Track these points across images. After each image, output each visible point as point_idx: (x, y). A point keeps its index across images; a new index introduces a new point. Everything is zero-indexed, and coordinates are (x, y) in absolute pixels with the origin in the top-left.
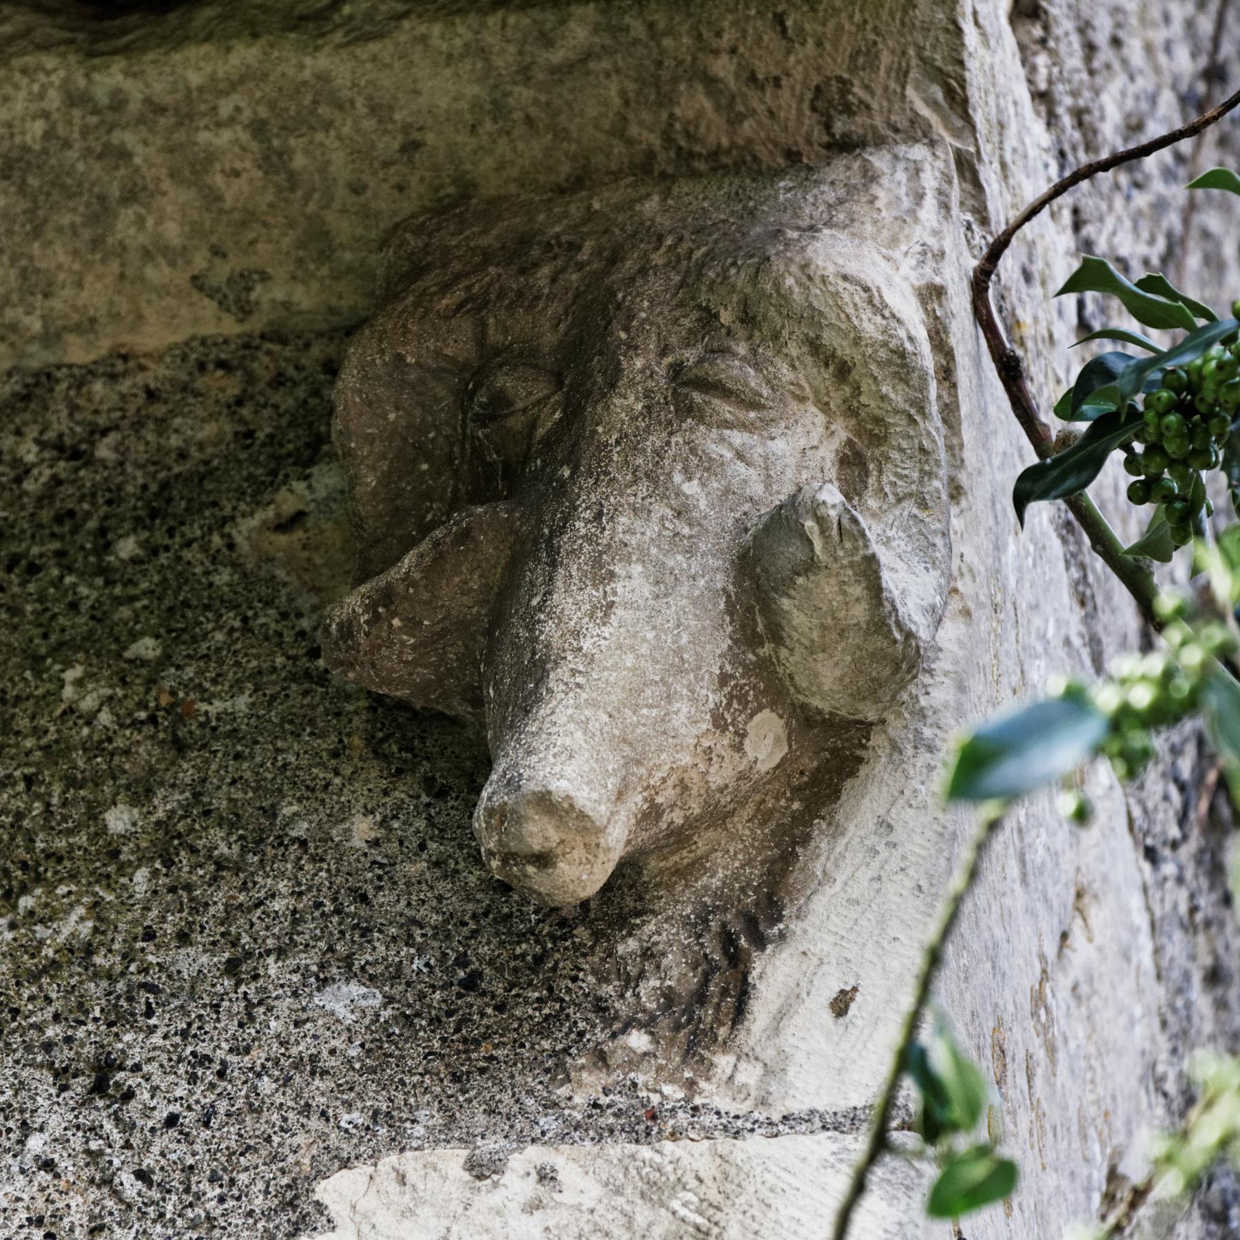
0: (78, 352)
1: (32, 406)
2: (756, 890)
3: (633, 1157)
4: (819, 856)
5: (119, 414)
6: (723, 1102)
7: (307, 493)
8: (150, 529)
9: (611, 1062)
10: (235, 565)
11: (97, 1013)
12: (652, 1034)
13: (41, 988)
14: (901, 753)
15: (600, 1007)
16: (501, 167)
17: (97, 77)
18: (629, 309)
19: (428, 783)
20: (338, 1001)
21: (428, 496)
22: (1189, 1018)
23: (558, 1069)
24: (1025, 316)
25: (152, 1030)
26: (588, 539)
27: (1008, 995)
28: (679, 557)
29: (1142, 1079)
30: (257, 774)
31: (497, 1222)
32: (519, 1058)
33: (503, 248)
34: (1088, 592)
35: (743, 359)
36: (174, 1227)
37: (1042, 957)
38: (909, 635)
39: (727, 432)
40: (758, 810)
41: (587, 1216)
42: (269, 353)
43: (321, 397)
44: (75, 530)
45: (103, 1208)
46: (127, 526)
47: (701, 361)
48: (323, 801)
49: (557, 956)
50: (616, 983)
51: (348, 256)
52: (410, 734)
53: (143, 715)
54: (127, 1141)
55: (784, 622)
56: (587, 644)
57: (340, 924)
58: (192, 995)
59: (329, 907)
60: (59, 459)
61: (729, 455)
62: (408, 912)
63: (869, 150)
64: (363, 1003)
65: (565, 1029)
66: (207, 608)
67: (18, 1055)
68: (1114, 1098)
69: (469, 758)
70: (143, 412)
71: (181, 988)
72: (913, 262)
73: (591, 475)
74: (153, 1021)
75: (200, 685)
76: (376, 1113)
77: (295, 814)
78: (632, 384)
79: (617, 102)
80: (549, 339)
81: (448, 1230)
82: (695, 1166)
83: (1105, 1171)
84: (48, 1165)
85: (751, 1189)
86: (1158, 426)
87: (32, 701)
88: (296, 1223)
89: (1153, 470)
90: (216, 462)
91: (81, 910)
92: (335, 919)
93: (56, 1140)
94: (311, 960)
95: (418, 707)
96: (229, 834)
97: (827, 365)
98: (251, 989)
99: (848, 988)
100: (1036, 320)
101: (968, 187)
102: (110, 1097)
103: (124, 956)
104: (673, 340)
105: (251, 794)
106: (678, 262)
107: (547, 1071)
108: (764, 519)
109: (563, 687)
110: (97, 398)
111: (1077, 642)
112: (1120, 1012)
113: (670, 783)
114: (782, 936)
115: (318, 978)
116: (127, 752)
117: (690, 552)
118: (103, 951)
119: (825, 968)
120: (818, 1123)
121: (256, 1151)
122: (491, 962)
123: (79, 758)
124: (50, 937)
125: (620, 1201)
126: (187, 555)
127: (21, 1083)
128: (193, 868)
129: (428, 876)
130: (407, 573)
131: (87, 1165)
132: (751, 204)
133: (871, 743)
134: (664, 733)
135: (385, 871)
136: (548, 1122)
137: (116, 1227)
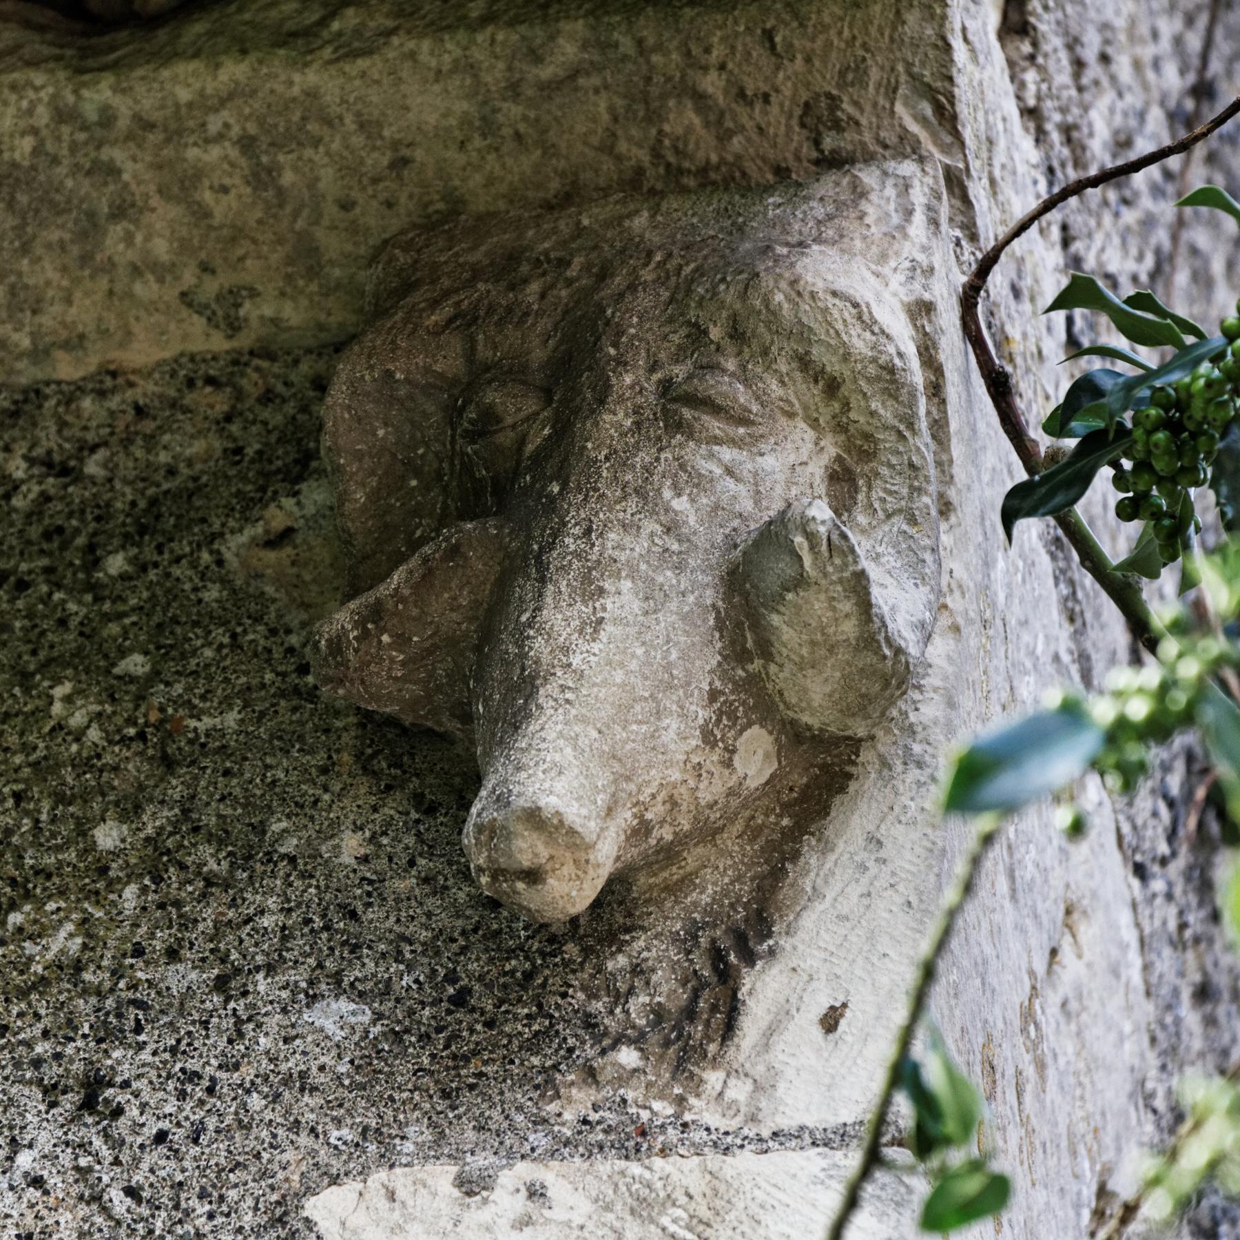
0: (67, 369)
1: (21, 422)
2: (746, 906)
3: (622, 1173)
5: (108, 430)
6: (713, 1119)
7: (295, 509)
8: (139, 545)
10: (225, 582)
11: (86, 1030)
12: (641, 1050)
13: (30, 1005)
15: (590, 1023)
16: (490, 181)
17: (86, 93)
19: (418, 799)
20: (327, 1018)
21: (416, 512)
22: (1178, 1034)
23: (547, 1085)
24: (1014, 332)
25: (141, 1046)
26: (577, 555)
27: (997, 1011)
28: (669, 573)
30: (247, 790)
32: (508, 1074)
33: (492, 264)
34: (1077, 609)
35: (733, 375)
37: (1032, 973)
38: (899, 651)
39: (716, 448)
40: (747, 826)
43: (310, 414)
44: (64, 547)
46: (116, 542)
47: (690, 377)
48: (312, 818)
49: (547, 972)
50: (606, 999)
51: (337, 272)
53: (132, 731)
54: (116, 1158)
55: (773, 638)
56: (576, 661)
57: (329, 940)
58: (182, 1011)
59: (318, 923)
60: (48, 475)
61: (718, 471)
63: (858, 166)
64: (353, 1020)
65: (555, 1046)
66: (196, 624)
67: (7, 1071)
68: (1103, 1114)
69: (457, 775)
71: (170, 1005)
72: (903, 278)
74: (142, 1038)
75: (189, 701)
76: (366, 1129)
77: (284, 831)
78: (621, 400)
79: (606, 117)
80: (538, 355)
82: (684, 1182)
84: (37, 1182)
85: (741, 1205)
86: (1147, 443)
87: (21, 718)
89: (1141, 487)
90: (204, 479)
91: (70, 927)
92: (325, 935)
93: (45, 1157)
94: (299, 977)
96: (218, 851)
97: (816, 381)
98: (240, 1005)
99: (838, 1004)
100: (1025, 335)
101: (958, 203)
102: (99, 1113)
103: (114, 973)
105: (240, 811)
106: (668, 278)
108: (753, 536)
109: (551, 703)
110: (86, 415)
111: (1066, 658)
112: (1109, 1029)
114: (772, 952)
115: (307, 995)
116: (115, 769)
117: (679, 568)
118: (92, 967)
119: (815, 984)
120: (808, 1140)
121: (246, 1167)
122: (481, 979)
123: (68, 775)
124: (40, 953)
125: (610, 1217)
126: (176, 571)
128: (182, 884)
129: (417, 891)
130: (396, 590)
131: (76, 1181)
132: (741, 220)
133: (861, 759)
134: (654, 749)
136: (538, 1139)
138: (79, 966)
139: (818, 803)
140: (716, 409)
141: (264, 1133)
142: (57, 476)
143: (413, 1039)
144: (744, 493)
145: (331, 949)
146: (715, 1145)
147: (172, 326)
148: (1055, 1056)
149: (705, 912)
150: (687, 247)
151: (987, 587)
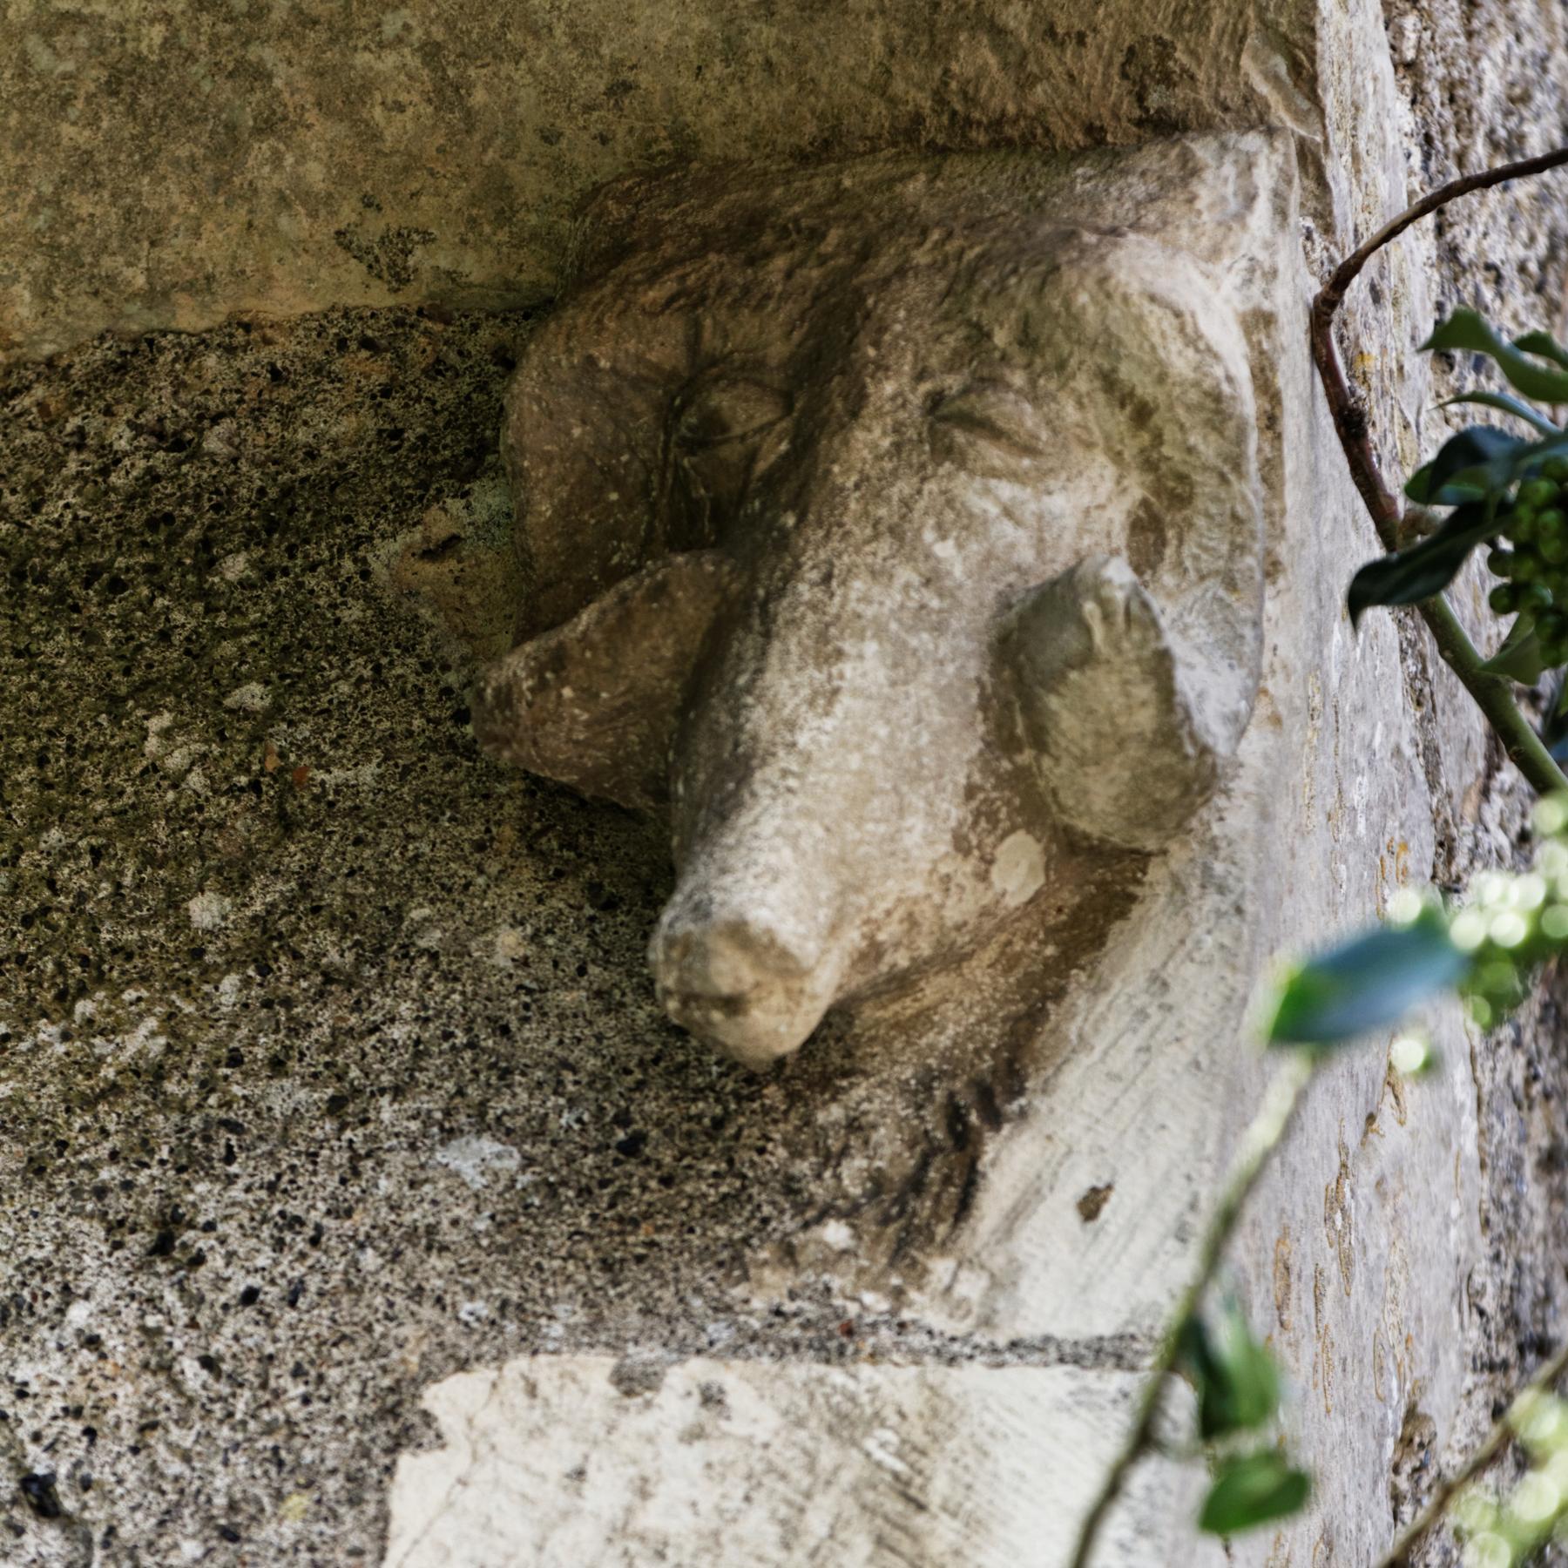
0: (189, 317)
2: (994, 1054)
3: (821, 1381)
4: (1074, 1016)
5: (236, 396)
6: (936, 1318)
7: (464, 513)
9: (801, 1259)
10: (369, 598)
11: (164, 1153)
12: (853, 1226)
13: (96, 1118)
14: (1184, 892)
15: (790, 1186)
16: (731, 120)
18: (881, 319)
19: (594, 889)
20: (465, 1159)
21: (614, 533)
22: (1517, 1216)
23: (735, 1263)
24: (1371, 346)
25: (231, 1180)
26: (814, 607)
27: (1297, 1196)
28: (925, 636)
29: (1456, 1293)
30: (382, 865)
31: (647, 1453)
32: (686, 1246)
33: (727, 229)
34: (1427, 690)
35: (1018, 392)
36: (245, 1430)
37: (1342, 1148)
38: (1204, 750)
39: (993, 482)
40: (1002, 953)
41: (759, 1452)
42: (426, 332)
43: (489, 394)
44: (171, 540)
45: (158, 1401)
46: (237, 539)
47: (966, 391)
48: (461, 905)
49: (742, 1120)
50: (813, 1159)
51: (533, 219)
52: (574, 828)
54: (193, 1319)
55: (1049, 725)
56: (803, 739)
57: (474, 1061)
58: (285, 1141)
59: (461, 1038)
60: (159, 448)
61: (994, 510)
62: (558, 1051)
63: (1190, 134)
64: (497, 1164)
65: (746, 1214)
66: (331, 650)
67: (63, 1201)
68: (1419, 1319)
69: (646, 863)
70: (266, 396)
71: (271, 1129)
72: (1238, 281)
73: (820, 524)
74: (234, 1169)
75: (317, 747)
76: (505, 1304)
77: (426, 919)
78: (879, 414)
79: (879, 49)
80: (778, 351)
81: (586, 1457)
82: (898, 1397)
83: (1402, 1412)
86: (1534, 524)
87: (106, 753)
88: (397, 1437)
89: (1523, 576)
91: (151, 1023)
92: (468, 1055)
93: (104, 1311)
94: (432, 1104)
95: (587, 795)
96: (342, 938)
97: (1123, 406)
98: (355, 1135)
99: (1101, 1185)
100: (1384, 349)
101: (1311, 185)
103: (203, 1084)
104: (934, 361)
105: (372, 890)
106: (946, 262)
107: (720, 1264)
108: (1033, 596)
109: (769, 791)
110: (209, 376)
111: (1409, 751)
112: (1433, 1212)
113: (896, 916)
114: (1023, 1114)
115: (442, 1129)
116: (220, 826)
117: (939, 629)
118: (176, 1076)
119: (1074, 1158)
120: (1053, 1354)
121: (353, 1341)
123: (161, 830)
124: (112, 1054)
125: (802, 1435)
126: (310, 581)
127: (65, 1236)
128: (295, 978)
129: (587, 1008)
130: (585, 633)
132: (1040, 194)
133: (1147, 879)
134: (893, 854)
135: (534, 997)
136: (720, 1331)
137: (172, 1427)
138: (159, 1074)
139: (1092, 929)
140: (995, 433)
141: (379, 1301)
142: (167, 450)
143: (571, 1194)
144: (1024, 541)
145: (476, 1072)
146: (938, 1353)
147: (324, 273)
148: (1365, 1248)
149: (943, 1058)
150: (972, 226)
151: (1319, 667)
